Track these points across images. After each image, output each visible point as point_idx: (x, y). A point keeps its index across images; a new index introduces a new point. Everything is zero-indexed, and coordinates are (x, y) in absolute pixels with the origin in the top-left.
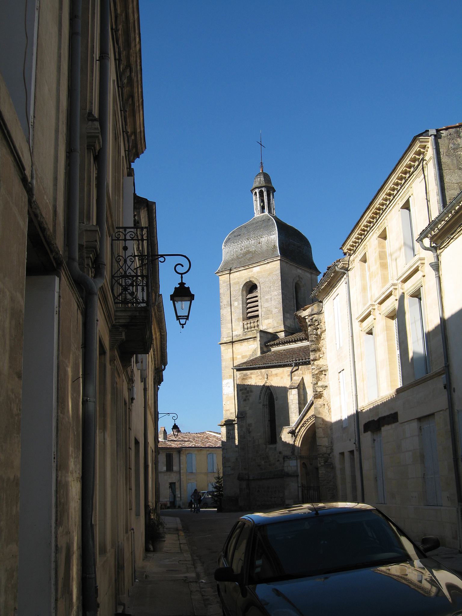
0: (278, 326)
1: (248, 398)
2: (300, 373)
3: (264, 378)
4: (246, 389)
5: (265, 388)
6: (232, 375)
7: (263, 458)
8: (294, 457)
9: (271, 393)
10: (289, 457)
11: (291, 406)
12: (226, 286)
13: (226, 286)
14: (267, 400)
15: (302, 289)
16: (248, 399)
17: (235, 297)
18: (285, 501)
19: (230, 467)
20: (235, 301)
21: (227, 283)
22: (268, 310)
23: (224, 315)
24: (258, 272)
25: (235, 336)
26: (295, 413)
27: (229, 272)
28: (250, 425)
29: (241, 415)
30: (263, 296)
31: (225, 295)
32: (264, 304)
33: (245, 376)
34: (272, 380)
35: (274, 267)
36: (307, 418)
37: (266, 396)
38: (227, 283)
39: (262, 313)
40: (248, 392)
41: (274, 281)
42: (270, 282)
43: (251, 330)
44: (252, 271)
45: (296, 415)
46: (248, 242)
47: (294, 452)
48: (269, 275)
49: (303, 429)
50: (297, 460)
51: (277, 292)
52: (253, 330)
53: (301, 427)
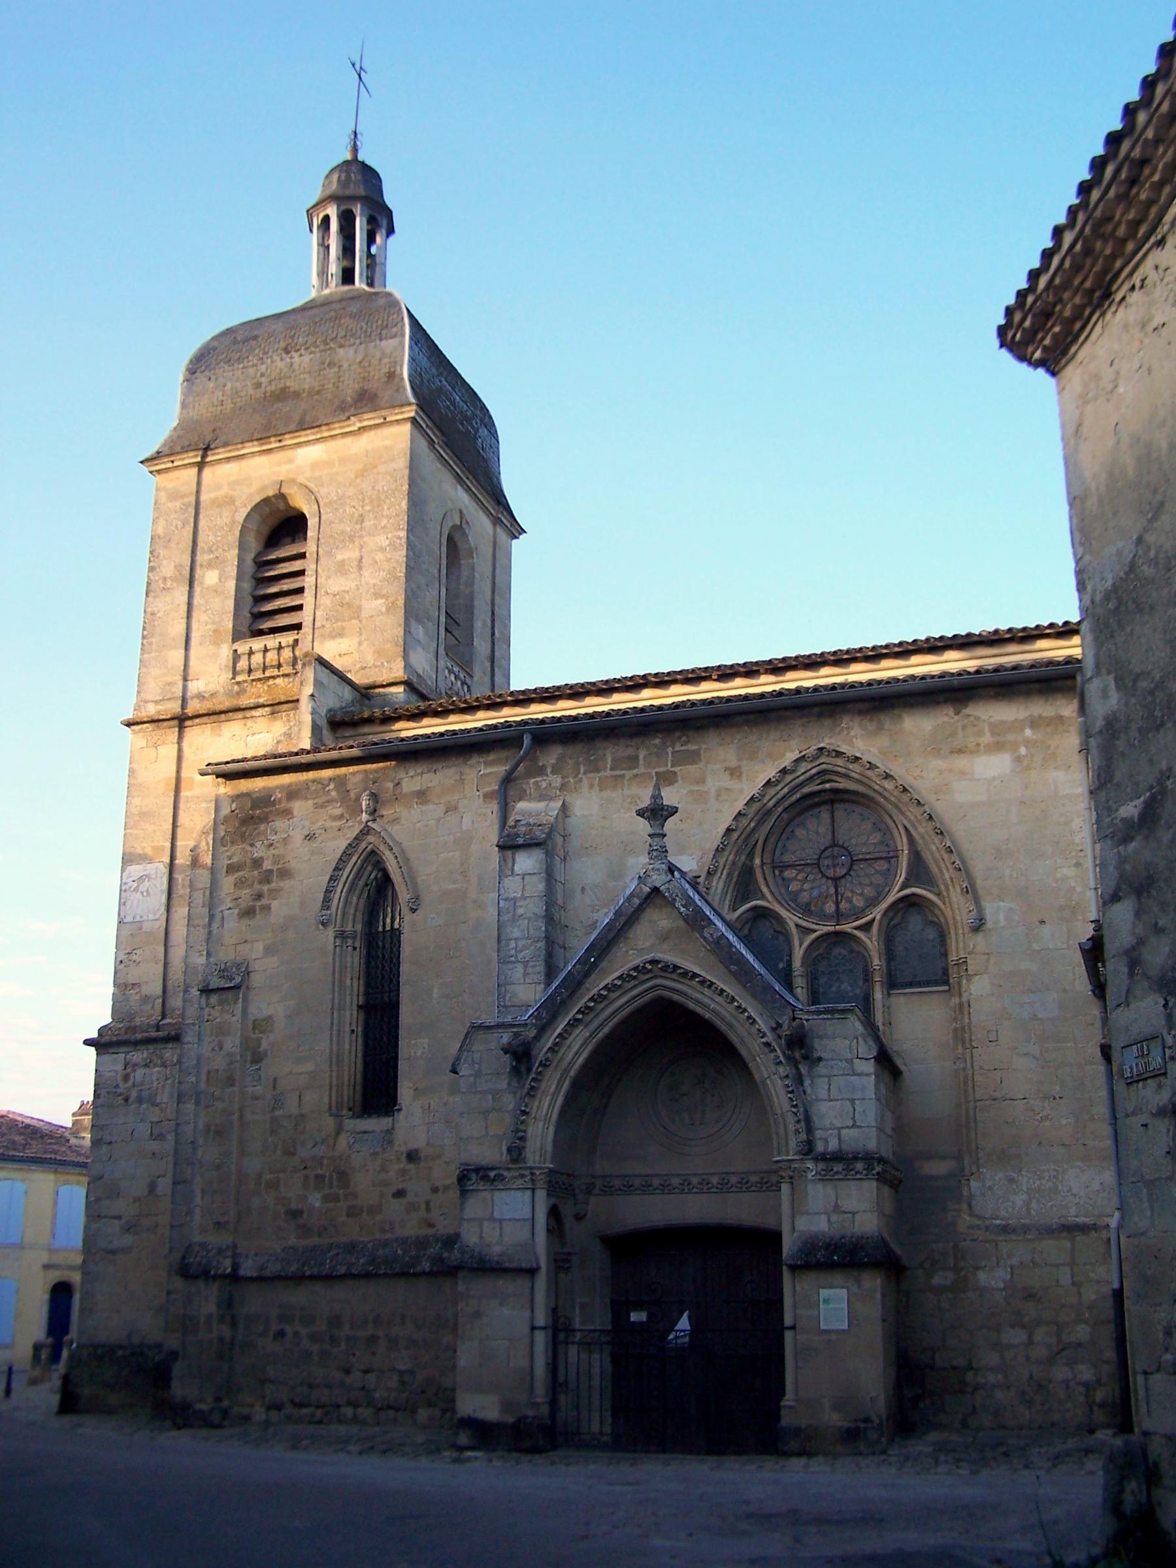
0: (379, 663)
1: (265, 901)
3: (356, 810)
4: (261, 866)
5: (354, 859)
6: (163, 846)
7: (317, 1176)
8: (522, 1176)
9: (384, 883)
10: (492, 1174)
12: (181, 508)
13: (181, 508)
14: (359, 916)
15: (462, 562)
16: (268, 908)
17: (211, 551)
19: (119, 1218)
20: (210, 565)
21: (186, 500)
22: (342, 605)
23: (159, 615)
24: (315, 465)
25: (192, 698)
26: (525, 964)
27: (199, 459)
28: (262, 1025)
29: (223, 977)
30: (329, 554)
31: (173, 545)
32: (330, 581)
33: (260, 808)
34: (396, 820)
35: (386, 448)
37: (357, 892)
38: (186, 500)
39: (318, 614)
40: (267, 877)
41: (379, 498)
42: (363, 500)
43: (262, 676)
44: (291, 461)
46: (288, 360)
47: (524, 1147)
48: (361, 474)
49: (579, 1036)
50: (533, 1190)
51: (389, 536)
52: (273, 677)
53: (574, 1023)
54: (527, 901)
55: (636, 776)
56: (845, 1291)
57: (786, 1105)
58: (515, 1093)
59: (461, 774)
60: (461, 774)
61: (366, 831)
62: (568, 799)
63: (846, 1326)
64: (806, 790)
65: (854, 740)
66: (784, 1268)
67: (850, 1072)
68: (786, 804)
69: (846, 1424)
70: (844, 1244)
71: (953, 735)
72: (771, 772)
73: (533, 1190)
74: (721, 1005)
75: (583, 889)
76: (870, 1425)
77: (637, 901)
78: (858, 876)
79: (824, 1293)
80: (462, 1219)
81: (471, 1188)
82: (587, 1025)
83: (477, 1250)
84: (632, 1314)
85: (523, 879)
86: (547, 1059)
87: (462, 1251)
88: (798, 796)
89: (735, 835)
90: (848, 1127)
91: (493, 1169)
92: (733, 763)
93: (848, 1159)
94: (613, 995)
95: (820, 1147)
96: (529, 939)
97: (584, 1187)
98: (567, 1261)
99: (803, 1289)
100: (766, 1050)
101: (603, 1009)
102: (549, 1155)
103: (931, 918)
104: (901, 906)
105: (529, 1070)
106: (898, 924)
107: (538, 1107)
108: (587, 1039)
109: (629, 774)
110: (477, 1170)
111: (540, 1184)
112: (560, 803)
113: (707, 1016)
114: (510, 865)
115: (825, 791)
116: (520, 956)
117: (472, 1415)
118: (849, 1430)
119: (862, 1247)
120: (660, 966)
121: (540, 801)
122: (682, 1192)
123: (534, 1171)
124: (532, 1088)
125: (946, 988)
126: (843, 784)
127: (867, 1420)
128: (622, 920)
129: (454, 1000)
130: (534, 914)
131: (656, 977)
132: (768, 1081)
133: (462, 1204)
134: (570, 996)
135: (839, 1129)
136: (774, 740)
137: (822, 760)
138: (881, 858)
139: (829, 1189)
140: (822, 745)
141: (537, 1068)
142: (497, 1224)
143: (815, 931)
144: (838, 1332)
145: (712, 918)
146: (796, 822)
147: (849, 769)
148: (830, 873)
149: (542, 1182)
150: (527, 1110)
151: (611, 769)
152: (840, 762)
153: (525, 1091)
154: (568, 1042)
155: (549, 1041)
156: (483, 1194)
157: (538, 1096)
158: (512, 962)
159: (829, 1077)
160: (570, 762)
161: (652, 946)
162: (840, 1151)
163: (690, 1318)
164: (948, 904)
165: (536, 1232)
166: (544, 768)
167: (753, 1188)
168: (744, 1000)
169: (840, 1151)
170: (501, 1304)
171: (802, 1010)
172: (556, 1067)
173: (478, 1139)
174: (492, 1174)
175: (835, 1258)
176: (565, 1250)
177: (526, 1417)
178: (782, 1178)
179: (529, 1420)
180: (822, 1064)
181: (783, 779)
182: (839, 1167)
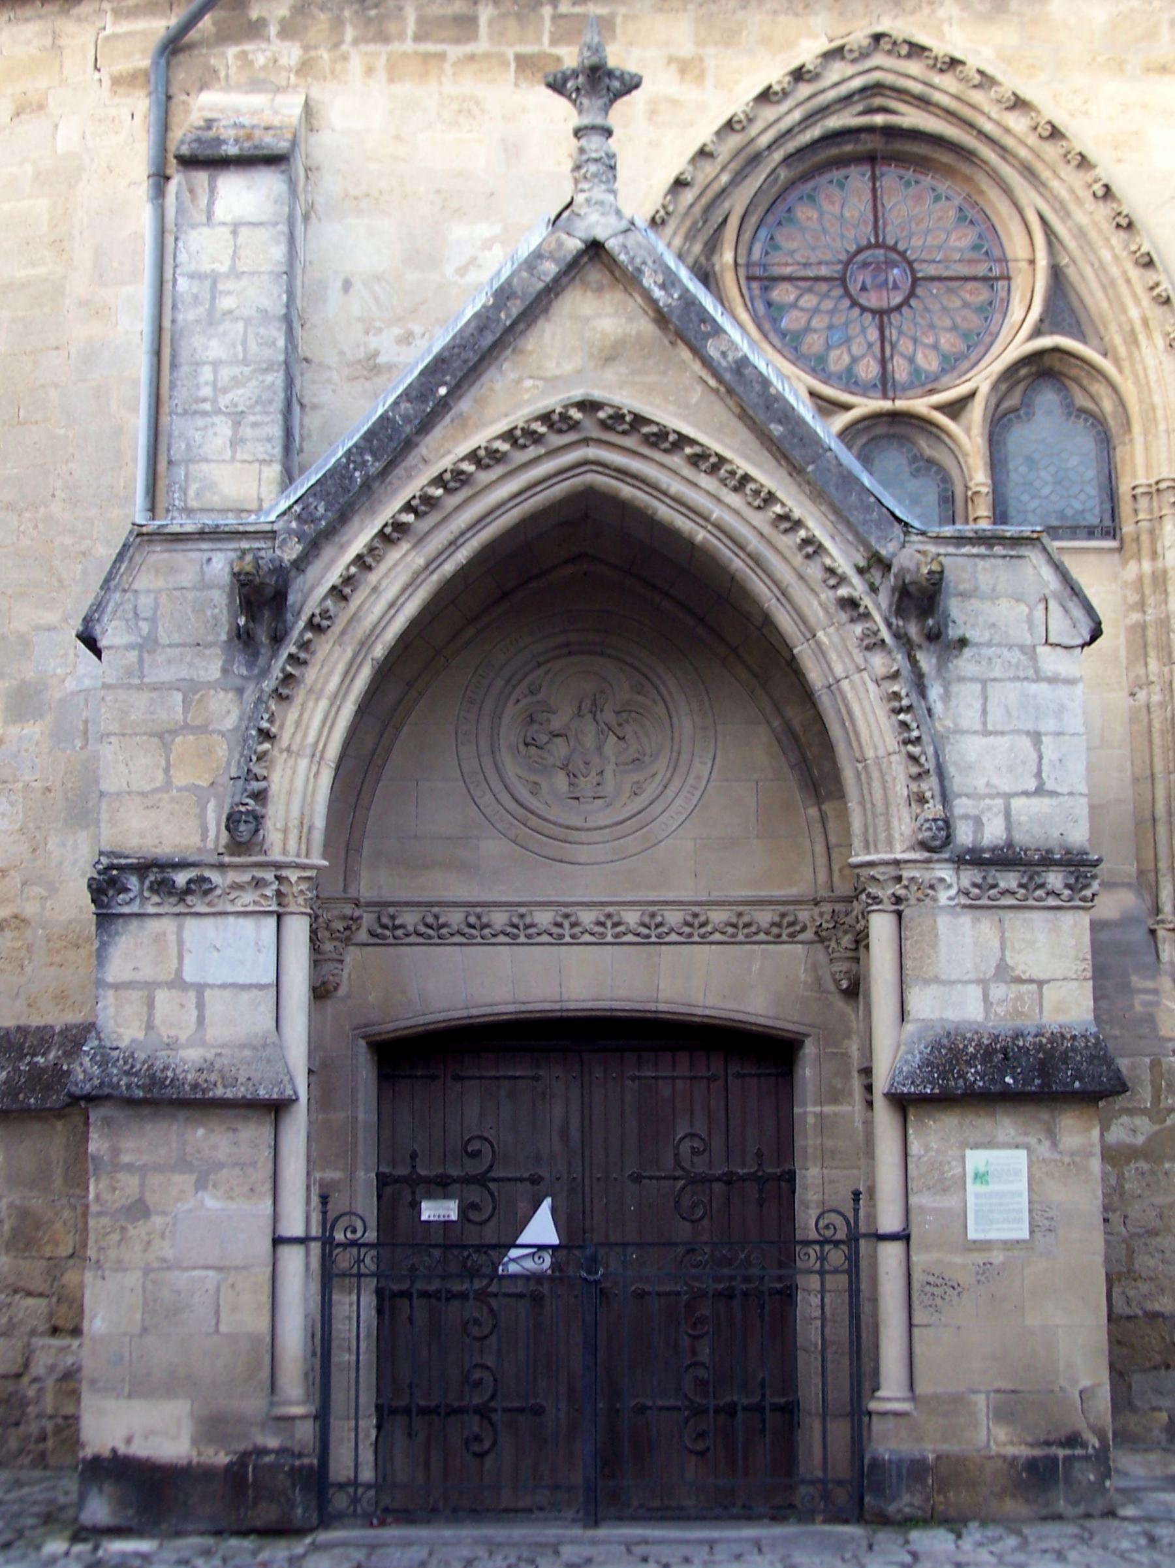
2: (283, 61)
8: (258, 883)
10: (181, 878)
11: (197, 341)
18: (71, 1421)
26: (237, 418)
36: (479, 439)
45: (248, 432)
50: (279, 917)
54: (244, 282)
55: (471, 58)
56: (1022, 1154)
57: (891, 741)
58: (240, 691)
59: (55, 36)
60: (55, 36)
62: (316, 93)
63: (1025, 1234)
64: (834, 122)
65: (946, 27)
67: (1031, 673)
68: (791, 146)
69: (1024, 1452)
70: (1025, 1051)
71: (1151, 35)
72: (775, 74)
73: (279, 917)
74: (736, 512)
75: (347, 285)
76: (1079, 1452)
77: (550, 269)
78: (927, 309)
79: (976, 1159)
80: (100, 983)
81: (126, 910)
82: (421, 540)
83: (141, 1055)
84: (424, 1205)
85: (234, 233)
86: (325, 615)
87: (103, 1058)
88: (815, 132)
89: (688, 196)
90: (1026, 794)
91: (183, 865)
92: (687, 49)
93: (1029, 864)
94: (484, 477)
95: (964, 836)
96: (245, 362)
97: (339, 925)
99: (928, 1149)
100: (843, 616)
101: (458, 508)
102: (318, 837)
103: (1082, 401)
104: (1023, 372)
105: (278, 639)
106: (1015, 410)
107: (298, 724)
108: (417, 574)
109: (455, 52)
110: (143, 868)
111: (297, 904)
112: (302, 99)
113: (701, 535)
114: (203, 201)
115: (870, 129)
116: (224, 401)
117: (122, 1450)
118: (1032, 1465)
119: (1065, 1058)
120: (602, 415)
121: (252, 91)
122: (559, 941)
123: (284, 873)
124: (288, 678)
125: (1114, 544)
126: (911, 118)
127: (1072, 1440)
128: (515, 308)
129: (27, 515)
130: (258, 310)
131: (586, 441)
132: (845, 684)
133: (104, 945)
134: (384, 473)
135: (1008, 797)
136: (775, 12)
137: (878, 59)
138: (975, 278)
139: (987, 927)
140: (879, 29)
141: (301, 634)
142: (192, 995)
144: (1008, 1245)
145: (719, 319)
146: (793, 195)
147: (932, 86)
148: (872, 300)
149: (301, 900)
150: (274, 730)
151: (417, 38)
152: (914, 67)
153: (268, 685)
154: (373, 578)
156: (154, 925)
157: (298, 700)
158: (205, 414)
159: (984, 682)
160: (322, 16)
161: (579, 372)
162: (1010, 845)
163: (554, 1211)
164: (1127, 371)
165: (284, 1013)
166: (262, 23)
167: (717, 937)
168: (793, 500)
169: (1010, 845)
170: (201, 1184)
171: (923, 533)
172: (343, 632)
173: (144, 794)
174: (181, 878)
175: (1009, 1080)
177: (262, 1451)
178: (876, 900)
179: (268, 1459)
180: (967, 652)
181: (793, 90)
182: (1009, 880)
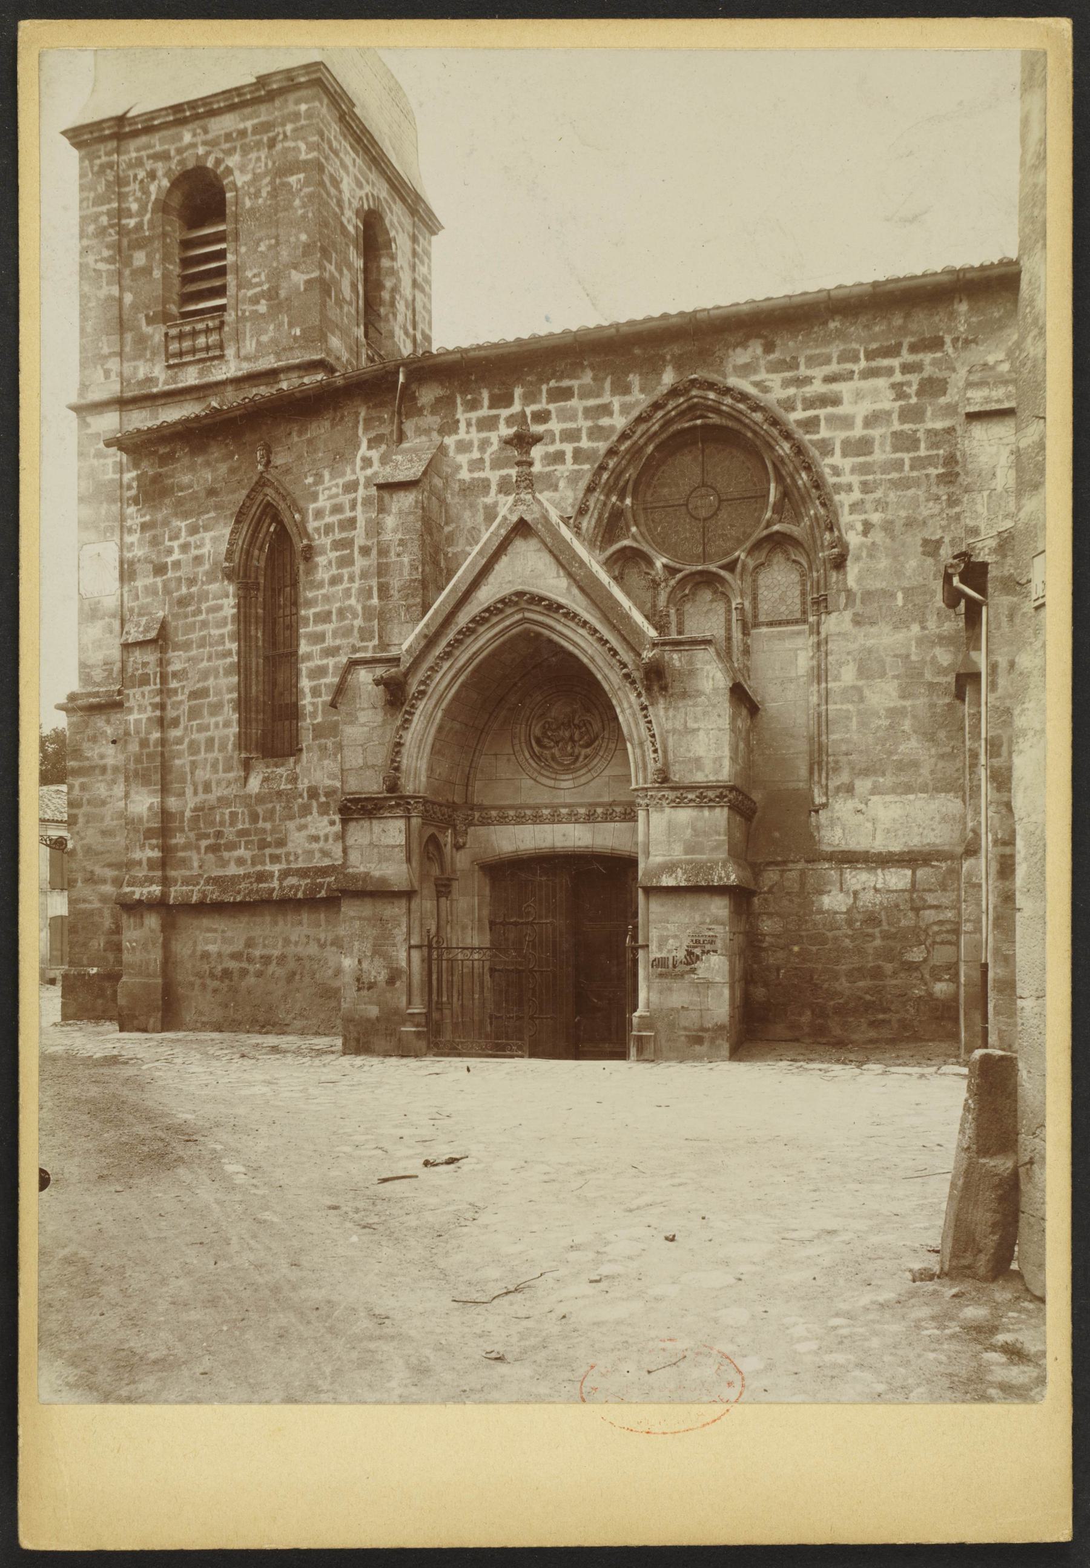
61: (262, 483)
66: (640, 890)
98: (448, 886)
131: (522, 610)
143: (680, 571)
155: (421, 675)
176: (446, 876)
